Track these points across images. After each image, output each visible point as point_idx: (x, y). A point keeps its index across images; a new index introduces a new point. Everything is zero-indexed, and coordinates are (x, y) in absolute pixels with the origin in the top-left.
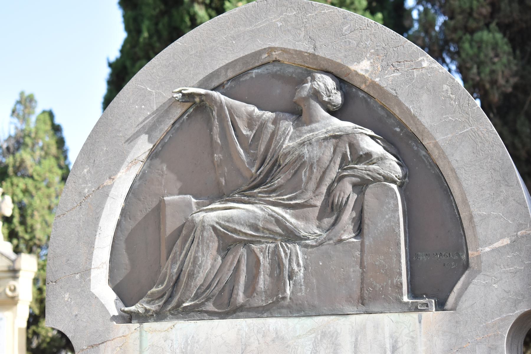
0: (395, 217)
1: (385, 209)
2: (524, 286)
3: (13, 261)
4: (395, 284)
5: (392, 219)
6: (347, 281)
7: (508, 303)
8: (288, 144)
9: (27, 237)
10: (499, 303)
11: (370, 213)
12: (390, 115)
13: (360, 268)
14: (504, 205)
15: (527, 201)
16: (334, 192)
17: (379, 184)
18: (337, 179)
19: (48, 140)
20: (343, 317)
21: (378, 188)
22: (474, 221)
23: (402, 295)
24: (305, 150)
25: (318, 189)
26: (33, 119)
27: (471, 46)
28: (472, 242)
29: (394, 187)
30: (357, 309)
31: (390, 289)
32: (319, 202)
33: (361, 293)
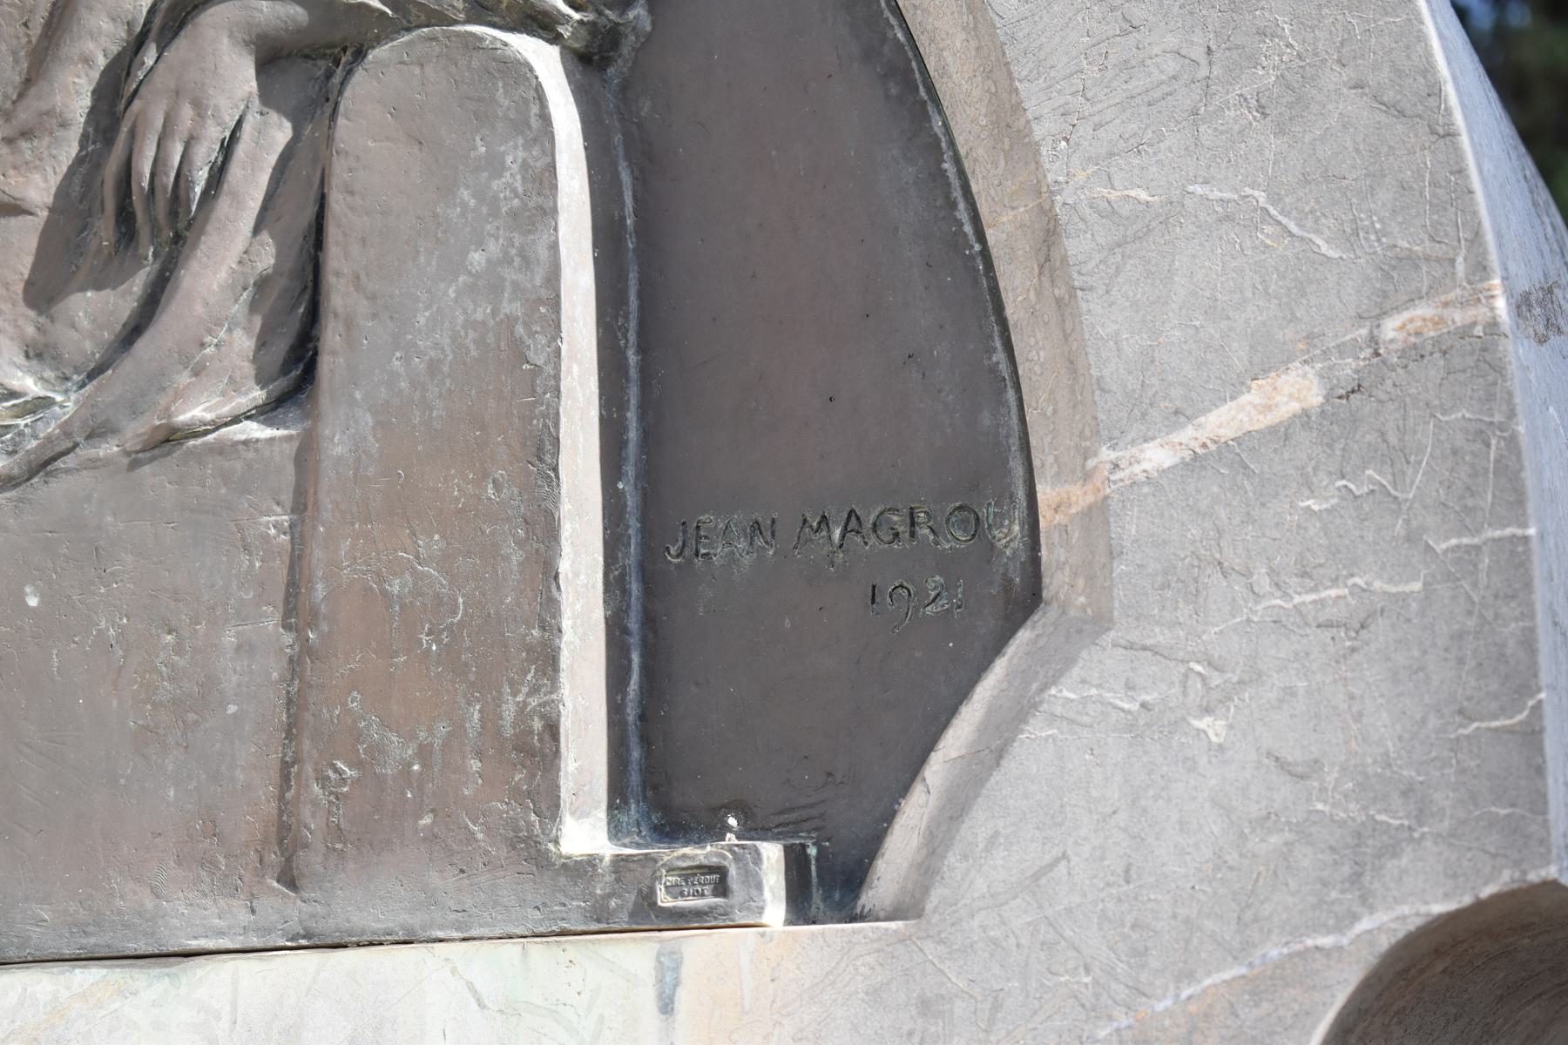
0: (527, 262)
1: (464, 205)
2: (1424, 721)
4: (509, 732)
5: (510, 275)
6: (192, 717)
7: (1305, 858)
10: (1232, 857)
11: (363, 241)
13: (287, 627)
14: (1280, 131)
15: (1450, 90)
16: (137, 105)
17: (434, 39)
18: (157, 21)
20: (156, 971)
21: (429, 69)
22: (1064, 259)
23: (550, 808)
25: (33, 91)
28: (1055, 411)
30: (253, 911)
31: (475, 765)
33: (281, 797)
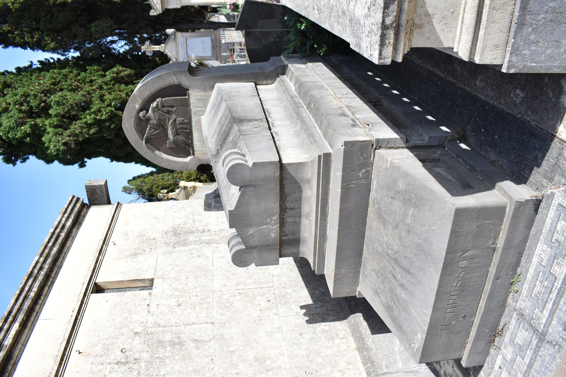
3: (182, 188)
8: (155, 122)
9: (173, 186)
12: (147, 100)
19: (138, 181)
24: (156, 118)
26: (131, 187)
27: (97, 34)
29: (163, 99)
32: (167, 115)
